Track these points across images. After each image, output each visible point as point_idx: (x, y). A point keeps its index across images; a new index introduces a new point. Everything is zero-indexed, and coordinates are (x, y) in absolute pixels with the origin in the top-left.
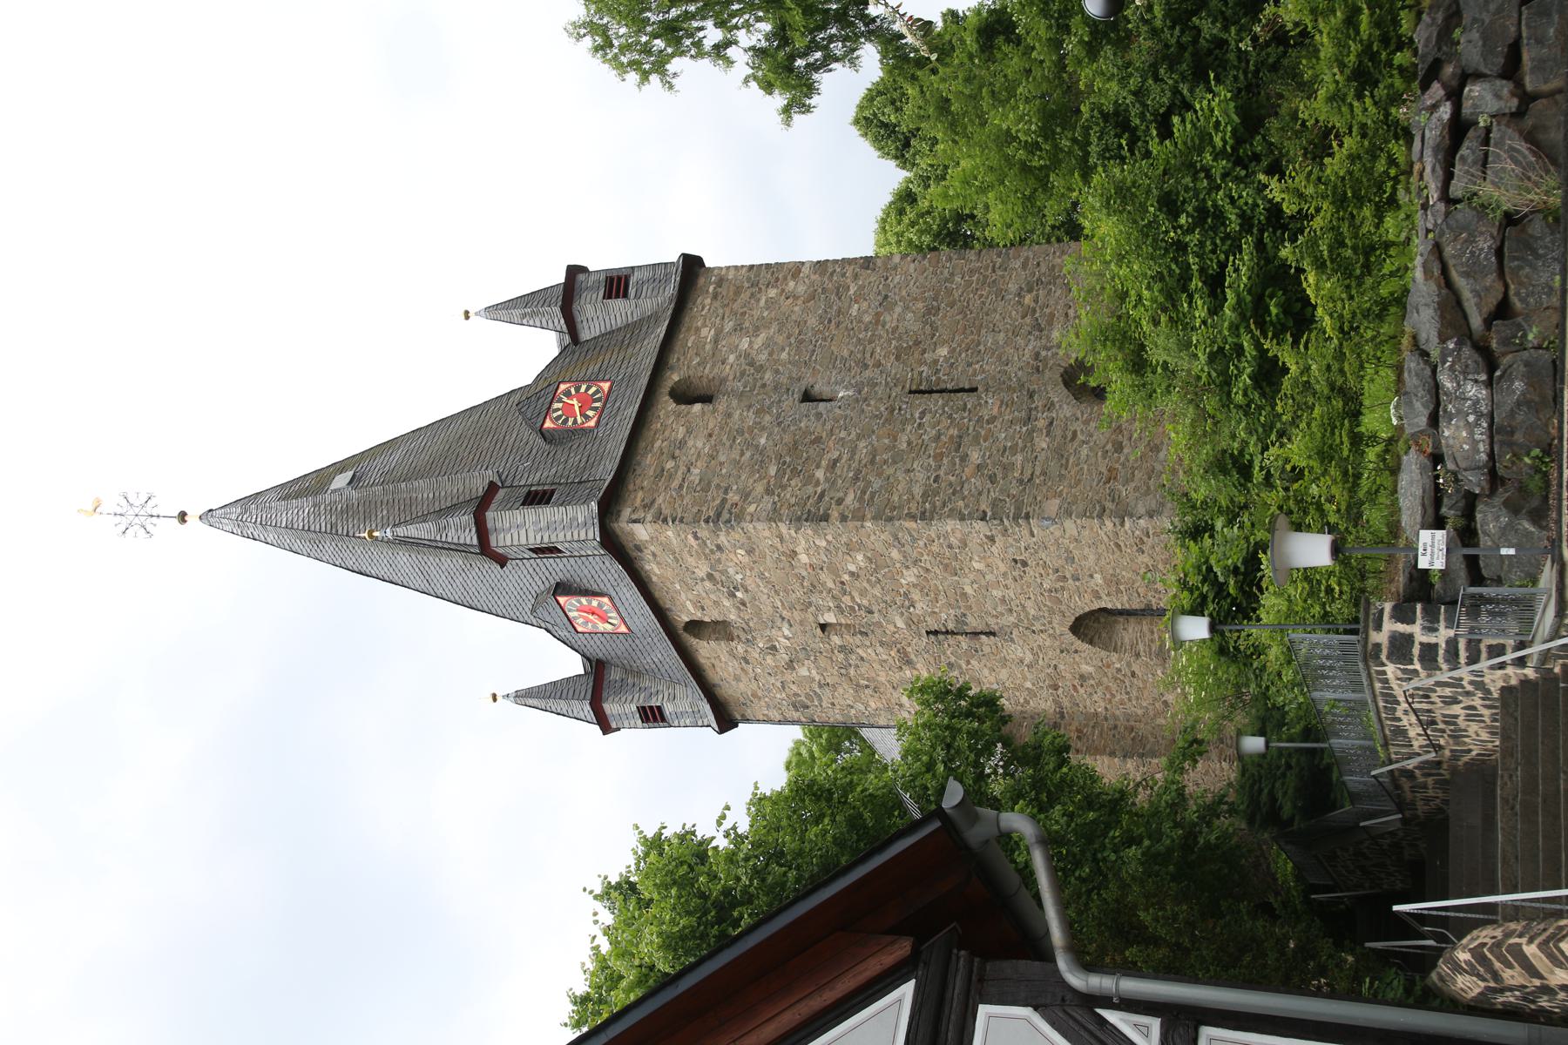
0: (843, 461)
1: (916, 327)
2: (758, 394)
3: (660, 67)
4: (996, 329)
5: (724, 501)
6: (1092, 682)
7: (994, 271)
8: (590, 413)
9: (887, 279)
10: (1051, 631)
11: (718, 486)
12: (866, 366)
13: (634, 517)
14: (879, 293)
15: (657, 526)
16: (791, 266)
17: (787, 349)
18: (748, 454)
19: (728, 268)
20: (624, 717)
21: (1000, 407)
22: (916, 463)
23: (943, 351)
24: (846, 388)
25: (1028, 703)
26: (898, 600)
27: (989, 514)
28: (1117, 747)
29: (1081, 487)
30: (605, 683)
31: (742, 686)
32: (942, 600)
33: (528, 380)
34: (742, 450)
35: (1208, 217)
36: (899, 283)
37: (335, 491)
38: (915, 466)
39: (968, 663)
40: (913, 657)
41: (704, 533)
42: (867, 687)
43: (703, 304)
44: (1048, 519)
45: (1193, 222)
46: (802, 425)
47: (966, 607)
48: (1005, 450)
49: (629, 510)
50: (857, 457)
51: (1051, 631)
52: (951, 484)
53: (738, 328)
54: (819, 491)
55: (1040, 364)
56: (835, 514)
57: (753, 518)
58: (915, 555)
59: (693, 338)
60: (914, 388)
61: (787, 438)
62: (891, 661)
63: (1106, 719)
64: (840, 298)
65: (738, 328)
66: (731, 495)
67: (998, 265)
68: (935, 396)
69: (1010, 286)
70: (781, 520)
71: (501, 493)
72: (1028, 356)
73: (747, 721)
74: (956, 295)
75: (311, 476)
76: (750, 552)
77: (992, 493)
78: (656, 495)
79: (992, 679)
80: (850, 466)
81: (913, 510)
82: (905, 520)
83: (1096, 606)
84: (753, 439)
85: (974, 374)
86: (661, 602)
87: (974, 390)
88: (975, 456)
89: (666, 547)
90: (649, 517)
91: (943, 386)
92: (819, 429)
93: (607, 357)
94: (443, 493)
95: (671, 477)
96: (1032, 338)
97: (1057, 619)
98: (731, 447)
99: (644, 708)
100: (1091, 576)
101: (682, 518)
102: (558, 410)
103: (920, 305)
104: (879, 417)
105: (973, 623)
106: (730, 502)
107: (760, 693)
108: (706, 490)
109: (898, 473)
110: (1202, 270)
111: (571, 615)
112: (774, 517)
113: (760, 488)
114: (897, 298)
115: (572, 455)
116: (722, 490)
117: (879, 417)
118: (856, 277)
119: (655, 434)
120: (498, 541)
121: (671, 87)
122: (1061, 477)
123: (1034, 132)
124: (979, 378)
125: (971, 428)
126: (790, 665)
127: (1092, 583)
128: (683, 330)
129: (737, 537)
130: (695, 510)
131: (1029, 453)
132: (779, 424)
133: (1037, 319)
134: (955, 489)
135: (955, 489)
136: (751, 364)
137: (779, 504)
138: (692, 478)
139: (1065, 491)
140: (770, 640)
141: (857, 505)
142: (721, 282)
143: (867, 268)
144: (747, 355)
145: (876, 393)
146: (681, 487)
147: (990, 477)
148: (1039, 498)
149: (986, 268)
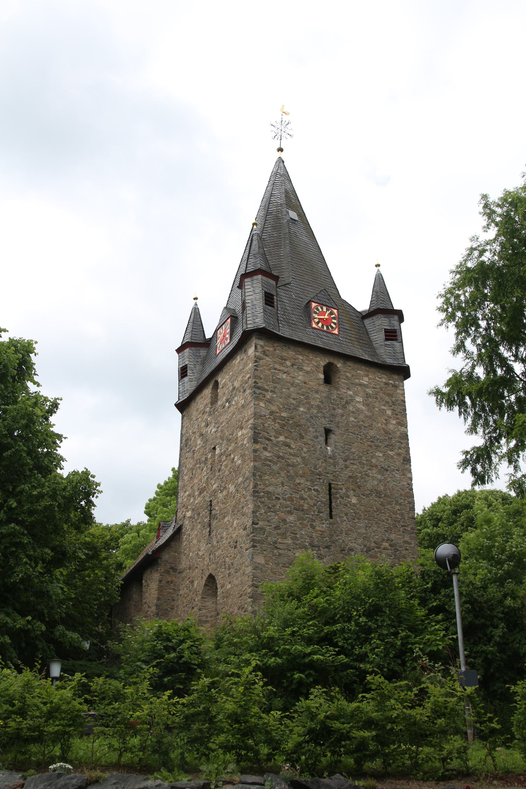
0: (289, 450)
1: (369, 486)
2: (329, 406)
3: (451, 317)
4: (367, 528)
5: (267, 391)
6: (191, 587)
7: (402, 526)
8: (320, 325)
9: (398, 471)
10: (210, 564)
11: (275, 387)
12: (345, 461)
13: (258, 347)
14: (389, 467)
15: (253, 358)
16: (404, 421)
17: (356, 420)
18: (294, 402)
19: (403, 390)
20: (183, 359)
21: (321, 531)
22: (288, 488)
23: (354, 500)
24: (332, 451)
25: (184, 555)
26: (223, 484)
27: (256, 526)
28: (162, 601)
29: (271, 574)
30: (199, 348)
31: (195, 412)
32: (222, 506)
33: (343, 297)
34: (296, 399)
35: (366, 635)
36: (395, 477)
37: (288, 212)
38: (286, 487)
39: (200, 523)
40: (203, 495)
41: (251, 382)
42: (192, 474)
43: (382, 378)
44: (253, 558)
45: (362, 626)
46: (311, 429)
47: (220, 519)
48: (294, 534)
49: (263, 344)
50: (291, 457)
51: (210, 564)
52: (274, 506)
53: (368, 396)
54: (271, 438)
55: (346, 551)
56: (258, 446)
57: (256, 406)
58: (240, 490)
59: (362, 373)
60: (332, 486)
61: (303, 422)
62: (201, 484)
63: (178, 595)
64: (386, 446)
65: (368, 396)
66: (270, 394)
67: (406, 528)
68: (328, 497)
69: (394, 535)
70: (255, 419)
71: (274, 283)
72: (351, 545)
73: (183, 418)
74: (388, 507)
75: (298, 203)
76: (243, 406)
77: (268, 527)
78: (271, 357)
79: (193, 536)
80: (286, 454)
81: (259, 487)
82: (254, 482)
83: (219, 586)
84: (303, 404)
85: (340, 517)
86: (225, 367)
87: (331, 517)
88: (291, 518)
89: (246, 364)
90: (257, 354)
91: (333, 501)
92: (308, 437)
93: (353, 332)
94: (282, 260)
95: (281, 364)
96: (362, 547)
97: (214, 566)
98: (298, 393)
99: (187, 368)
100: (230, 583)
101: (257, 370)
102: (322, 309)
103: (382, 488)
104: (315, 468)
105: (214, 523)
106: (266, 393)
107: (192, 422)
108: (273, 381)
109: (281, 479)
110: (334, 633)
111: (224, 326)
112: (256, 415)
113: (274, 408)
114: (386, 476)
115: (297, 317)
116: (273, 389)
117: (315, 468)
118: (399, 454)
119: (306, 356)
120: (248, 282)
121: (441, 325)
122: (278, 564)
123: (511, 550)
124: (338, 519)
125: (308, 516)
126: (201, 435)
127: (227, 583)
128: (367, 368)
129: (249, 398)
130: (262, 376)
131: (292, 547)
132: (311, 417)
133: (373, 549)
134: (271, 508)
135: (271, 508)
136: (347, 403)
137: (264, 418)
138: (280, 374)
139: (269, 566)
140: (211, 423)
141: (263, 458)
142: (396, 387)
143: (404, 460)
144: (352, 400)
145: (329, 466)
146: (276, 369)
147: (278, 526)
148: (265, 552)
149: (404, 522)
